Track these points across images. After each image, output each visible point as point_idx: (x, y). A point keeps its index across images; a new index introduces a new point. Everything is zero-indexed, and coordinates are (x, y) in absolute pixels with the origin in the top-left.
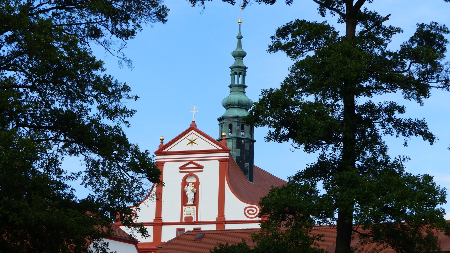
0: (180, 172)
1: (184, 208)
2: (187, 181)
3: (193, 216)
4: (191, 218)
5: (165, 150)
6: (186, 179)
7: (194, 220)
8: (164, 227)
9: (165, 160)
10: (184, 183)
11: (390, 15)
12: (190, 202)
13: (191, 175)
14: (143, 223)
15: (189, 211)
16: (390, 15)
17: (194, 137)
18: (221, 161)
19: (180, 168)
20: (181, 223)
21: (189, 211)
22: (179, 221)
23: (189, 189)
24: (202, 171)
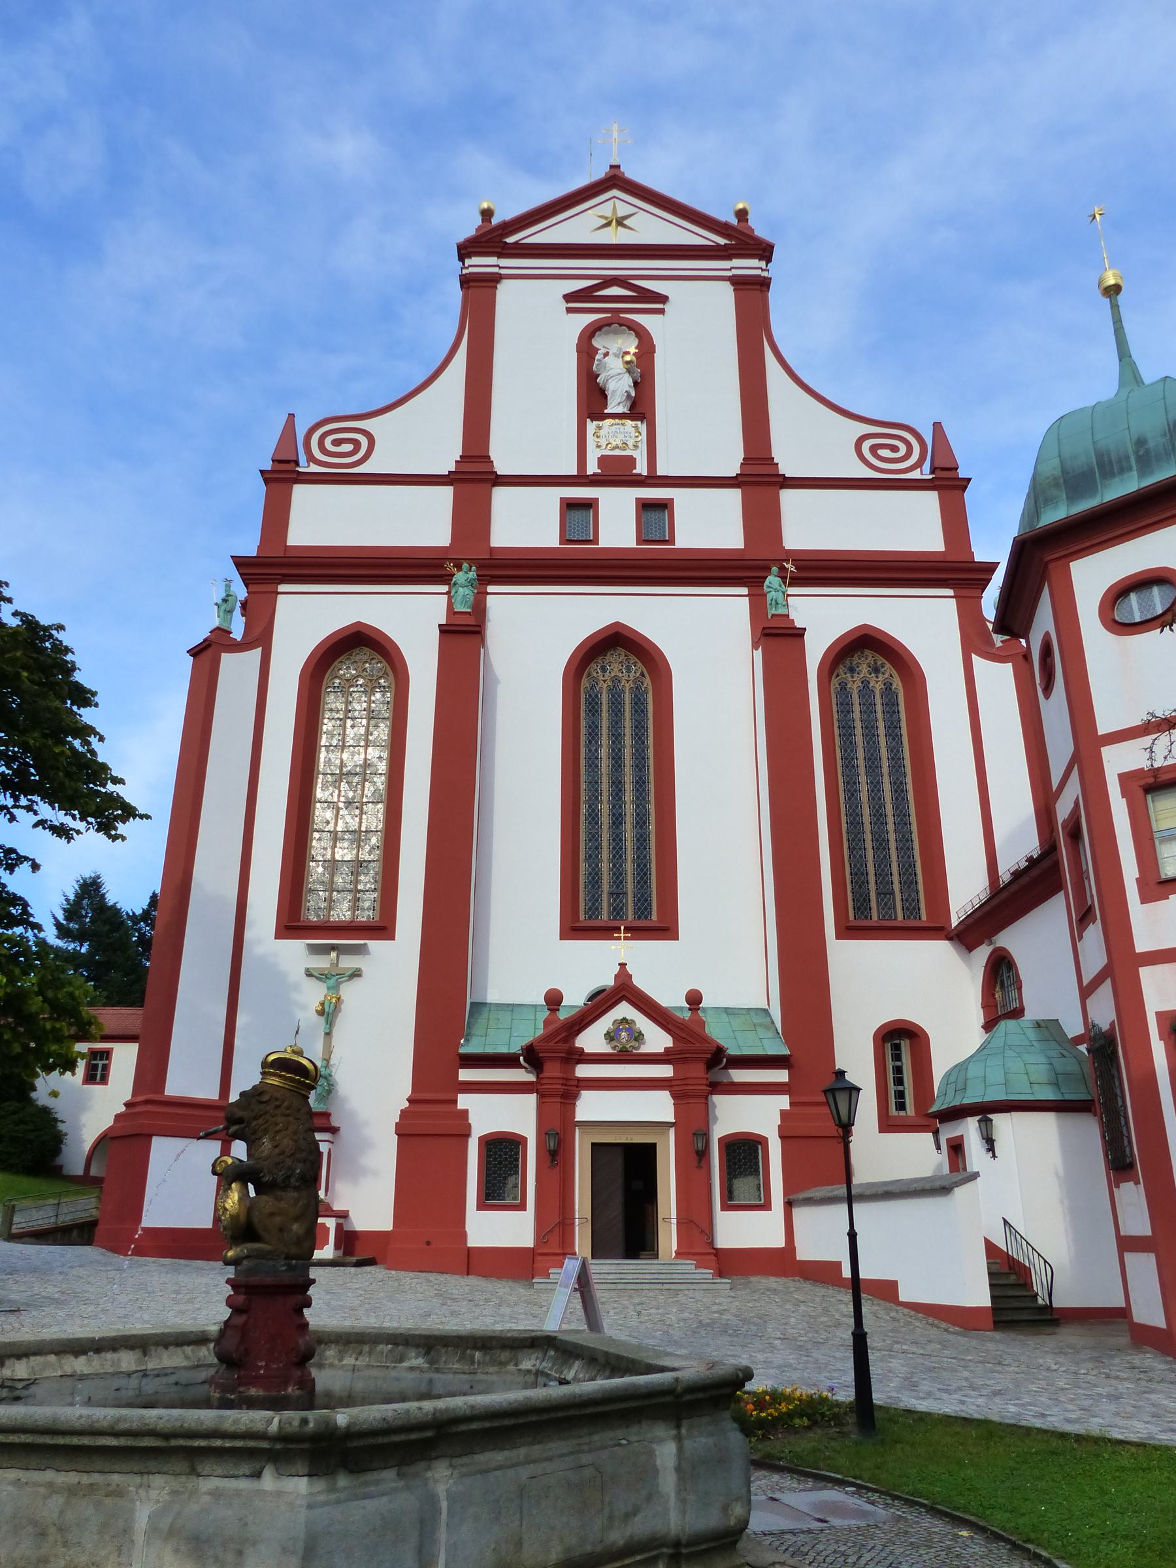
0: (569, 310)
1: (591, 426)
2: (597, 342)
3: (635, 454)
4: (631, 461)
5: (511, 240)
6: (592, 335)
7: (641, 469)
8: (500, 495)
9: (503, 272)
10: (586, 351)
11: (994, 1156)
12: (616, 405)
13: (614, 323)
14: (997, 1343)
15: (615, 436)
16: (994, 1156)
17: (623, 210)
18: (739, 283)
19: (568, 298)
20: (581, 479)
21: (615, 436)
22: (570, 468)
23: (615, 354)
24: (661, 311)
